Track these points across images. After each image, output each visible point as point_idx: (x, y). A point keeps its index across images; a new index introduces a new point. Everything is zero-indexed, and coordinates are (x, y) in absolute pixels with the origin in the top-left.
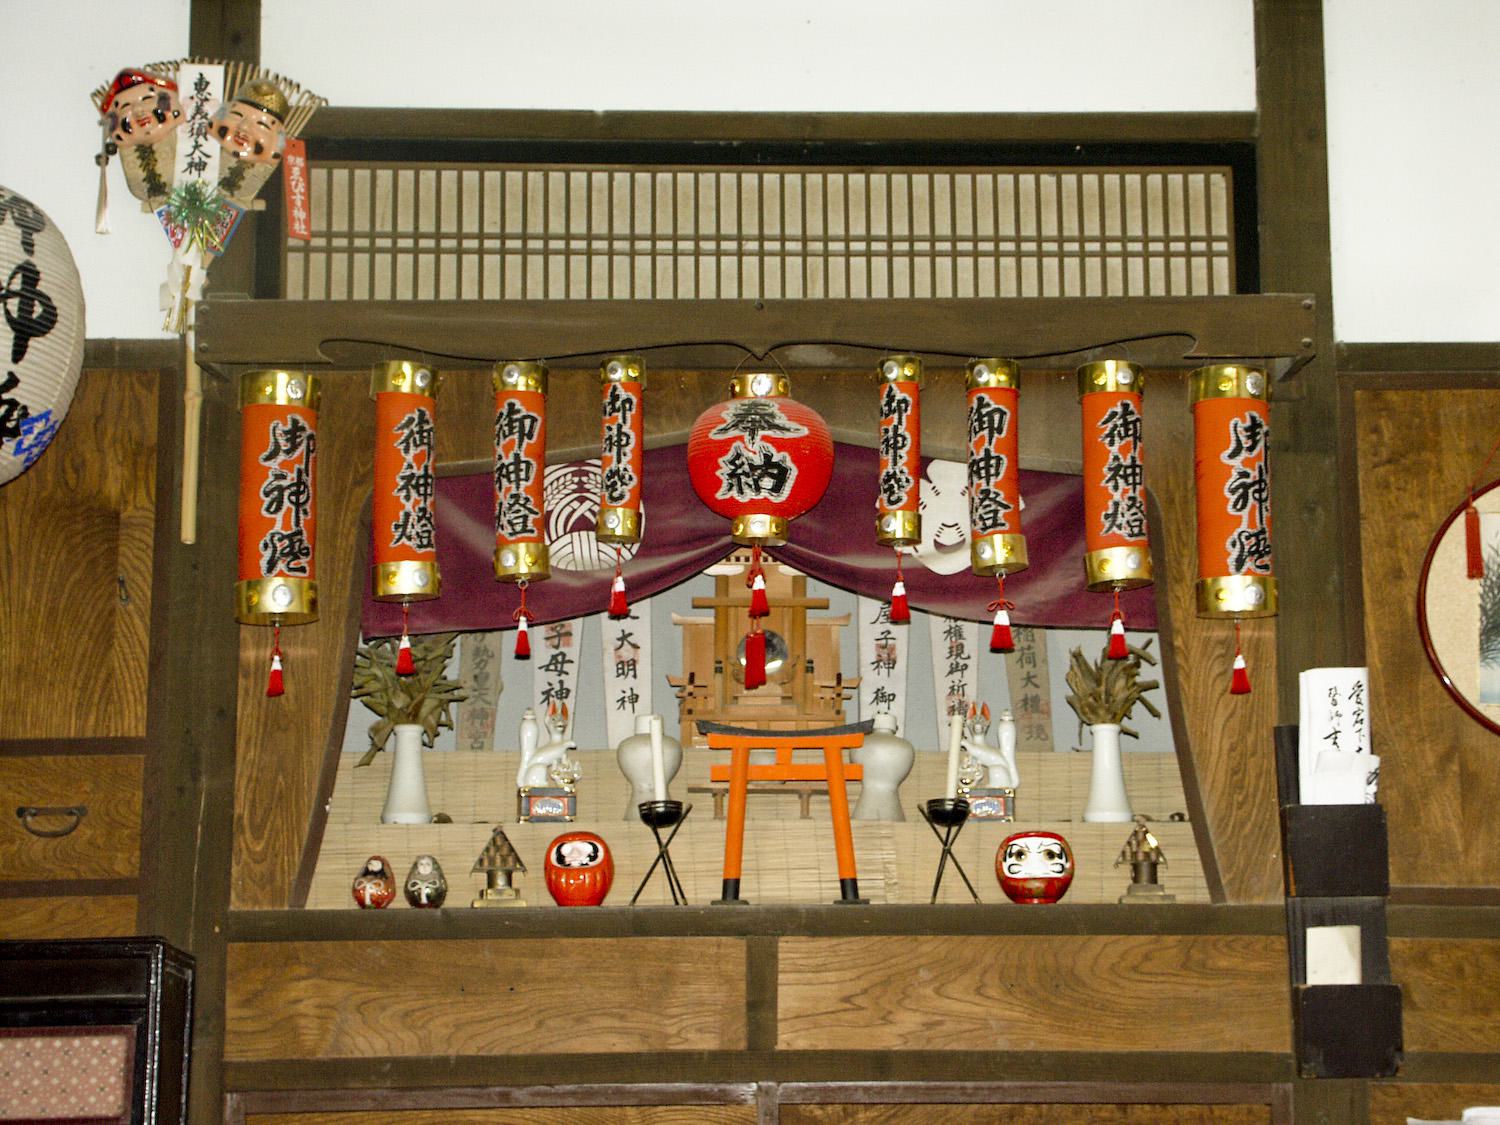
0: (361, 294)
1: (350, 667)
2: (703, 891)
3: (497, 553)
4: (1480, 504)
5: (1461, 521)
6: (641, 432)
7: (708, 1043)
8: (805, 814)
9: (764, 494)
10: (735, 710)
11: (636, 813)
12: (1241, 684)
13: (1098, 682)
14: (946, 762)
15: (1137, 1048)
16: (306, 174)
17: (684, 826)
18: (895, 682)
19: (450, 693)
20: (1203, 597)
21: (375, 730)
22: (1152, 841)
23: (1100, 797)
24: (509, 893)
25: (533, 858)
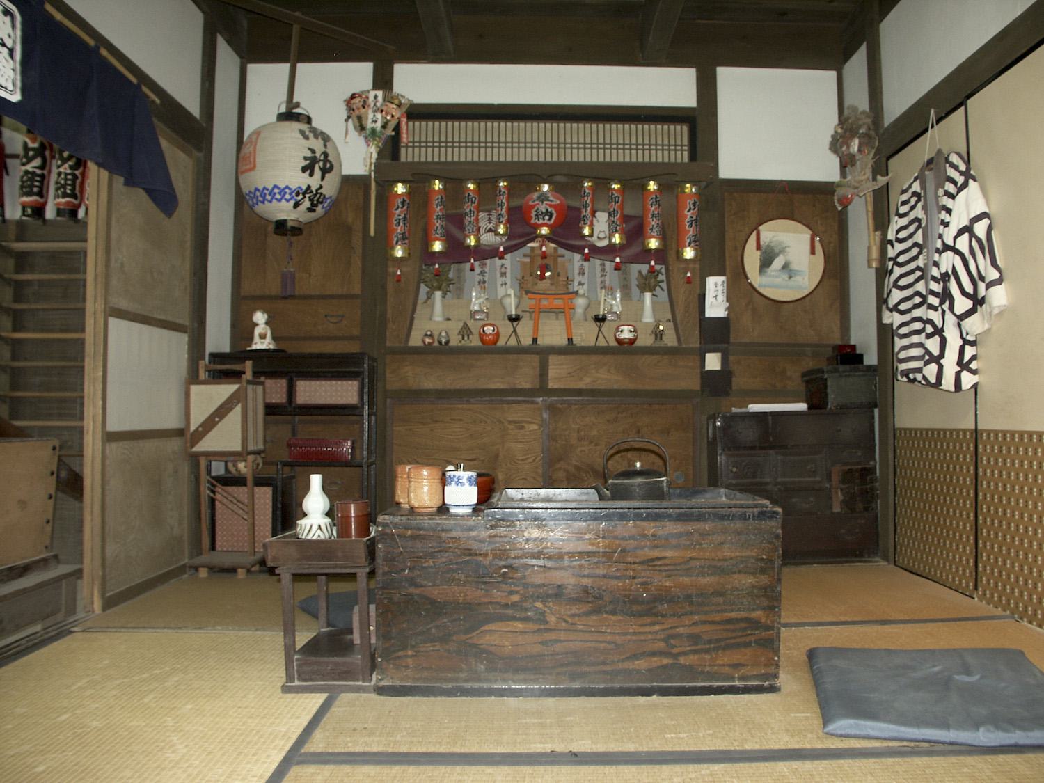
0: (423, 159)
1: (420, 274)
2: (527, 341)
3: (464, 239)
4: (761, 228)
5: (755, 233)
6: (508, 202)
7: (528, 386)
8: (557, 319)
9: (546, 221)
10: (536, 287)
11: (506, 318)
12: (689, 281)
13: (646, 280)
14: (599, 304)
15: (655, 388)
16: (407, 124)
17: (521, 322)
18: (585, 280)
19: (450, 282)
20: (679, 254)
21: (428, 293)
22: (661, 328)
23: (643, 315)
24: (468, 342)
25: (475, 331)
